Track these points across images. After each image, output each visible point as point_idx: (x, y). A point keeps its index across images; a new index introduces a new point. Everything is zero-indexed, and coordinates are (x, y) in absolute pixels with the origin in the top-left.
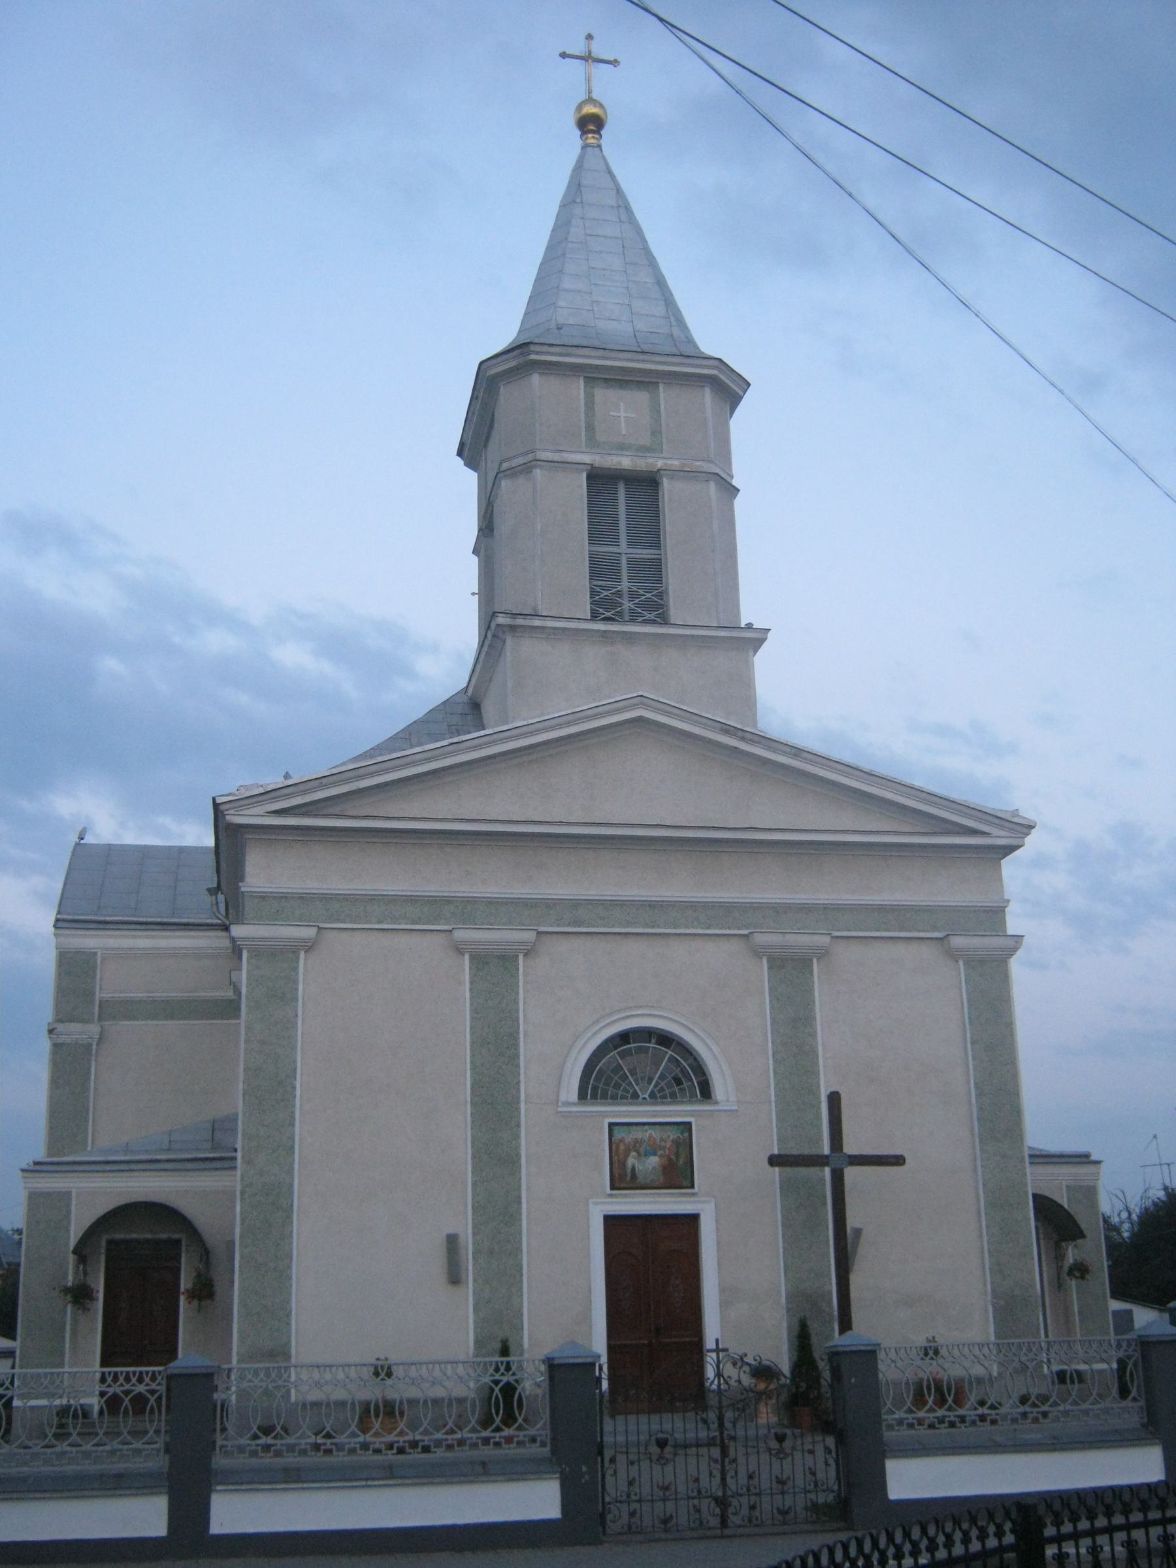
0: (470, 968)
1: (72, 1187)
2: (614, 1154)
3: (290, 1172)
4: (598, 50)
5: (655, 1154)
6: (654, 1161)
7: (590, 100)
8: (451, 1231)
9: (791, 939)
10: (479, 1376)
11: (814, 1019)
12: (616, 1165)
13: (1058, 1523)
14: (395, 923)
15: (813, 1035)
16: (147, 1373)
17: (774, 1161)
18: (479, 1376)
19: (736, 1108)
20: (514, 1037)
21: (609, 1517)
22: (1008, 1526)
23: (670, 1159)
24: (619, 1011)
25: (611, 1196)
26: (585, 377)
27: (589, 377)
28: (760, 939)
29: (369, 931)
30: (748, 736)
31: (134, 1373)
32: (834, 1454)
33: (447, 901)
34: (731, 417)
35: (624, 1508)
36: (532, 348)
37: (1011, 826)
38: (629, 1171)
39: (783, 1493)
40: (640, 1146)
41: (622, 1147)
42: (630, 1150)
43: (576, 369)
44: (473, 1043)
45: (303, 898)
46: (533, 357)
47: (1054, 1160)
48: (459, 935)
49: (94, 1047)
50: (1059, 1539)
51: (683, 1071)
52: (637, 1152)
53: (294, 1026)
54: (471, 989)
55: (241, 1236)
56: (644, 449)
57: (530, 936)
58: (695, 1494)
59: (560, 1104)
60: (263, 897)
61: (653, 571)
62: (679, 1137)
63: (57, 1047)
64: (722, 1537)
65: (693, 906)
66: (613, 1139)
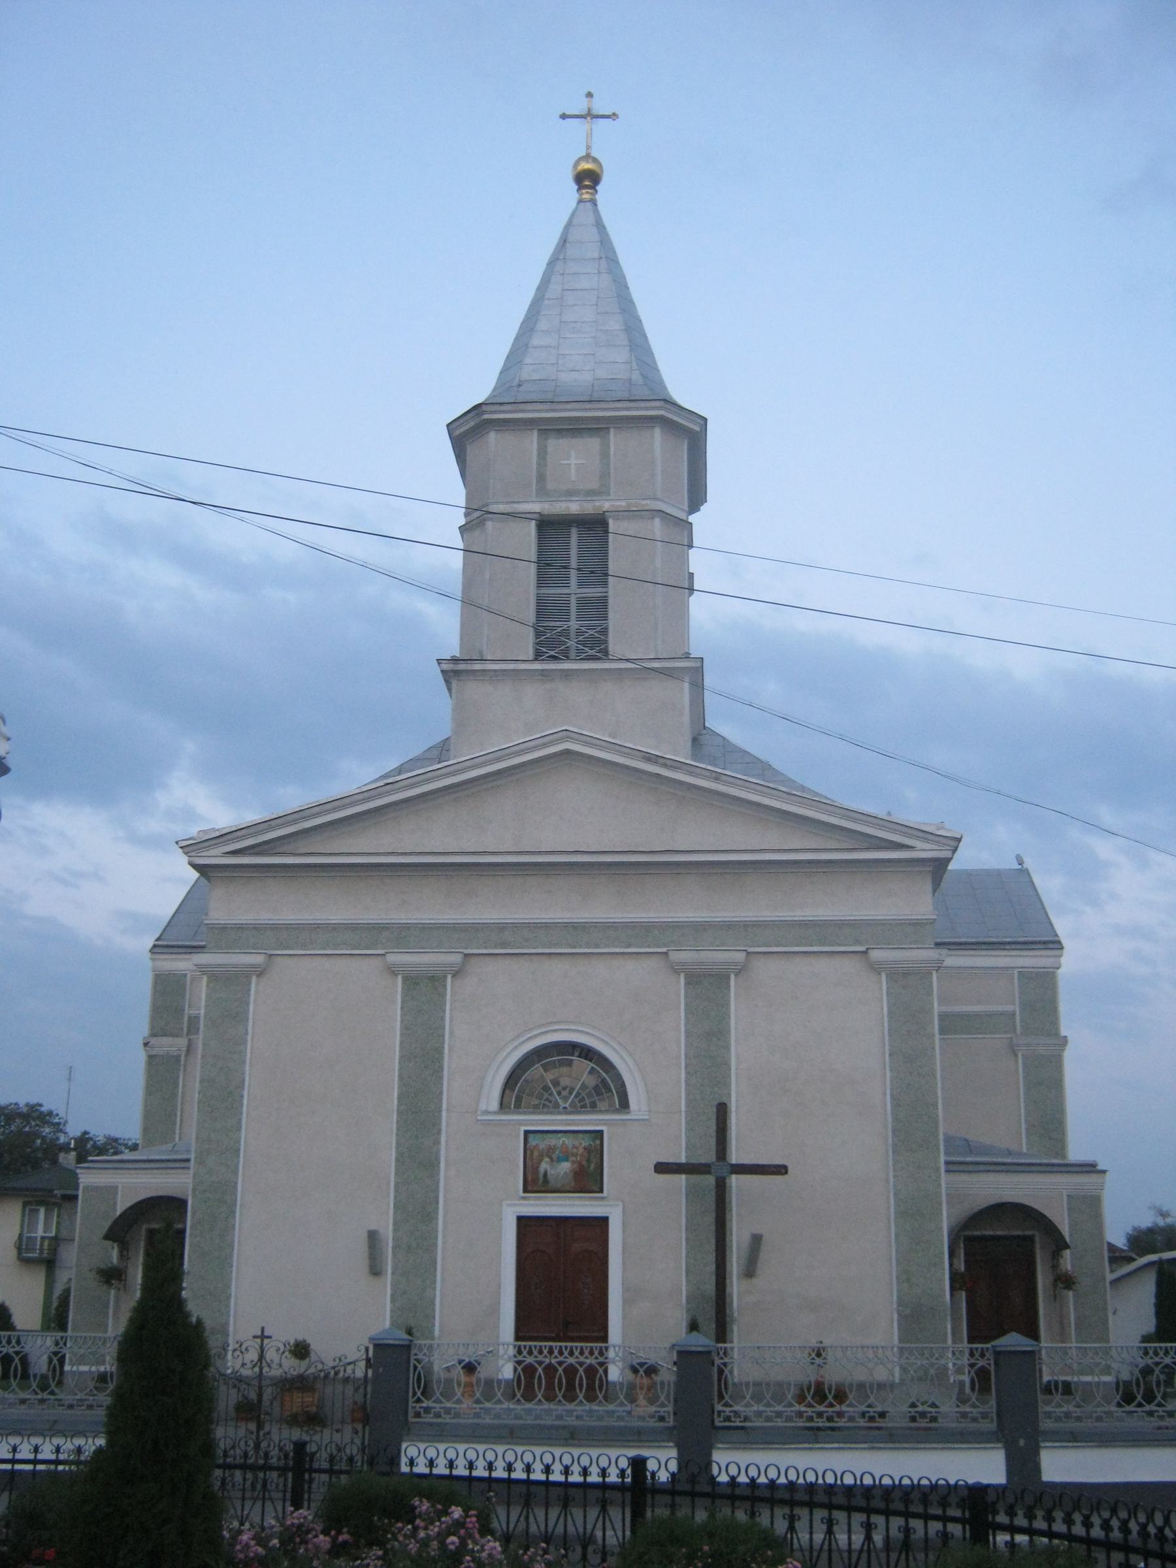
2: (528, 1160)
3: (236, 1172)
4: (599, 107)
5: (567, 1160)
6: (566, 1166)
7: (588, 157)
8: (372, 1228)
9: (705, 956)
10: (813, 1359)
11: (729, 1031)
12: (529, 1163)
15: (728, 1048)
16: (577, 1347)
18: (813, 1359)
19: (647, 1117)
20: (439, 1051)
24: (540, 1026)
25: (524, 1198)
26: (539, 430)
27: (542, 430)
28: (675, 956)
29: (363, 957)
30: (669, 763)
31: (525, 1347)
32: (360, 1435)
36: (484, 408)
37: (937, 838)
41: (536, 1154)
42: (543, 1156)
43: (529, 423)
44: (401, 1057)
45: (257, 928)
46: (486, 416)
47: (1033, 1168)
48: (391, 958)
49: (183, 1058)
51: (604, 1081)
53: (245, 1042)
54: (402, 1008)
55: (191, 1227)
56: (591, 493)
57: (457, 959)
59: (479, 1113)
61: (598, 608)
62: (591, 1145)
63: (151, 1058)
65: (613, 926)
66: (528, 1145)
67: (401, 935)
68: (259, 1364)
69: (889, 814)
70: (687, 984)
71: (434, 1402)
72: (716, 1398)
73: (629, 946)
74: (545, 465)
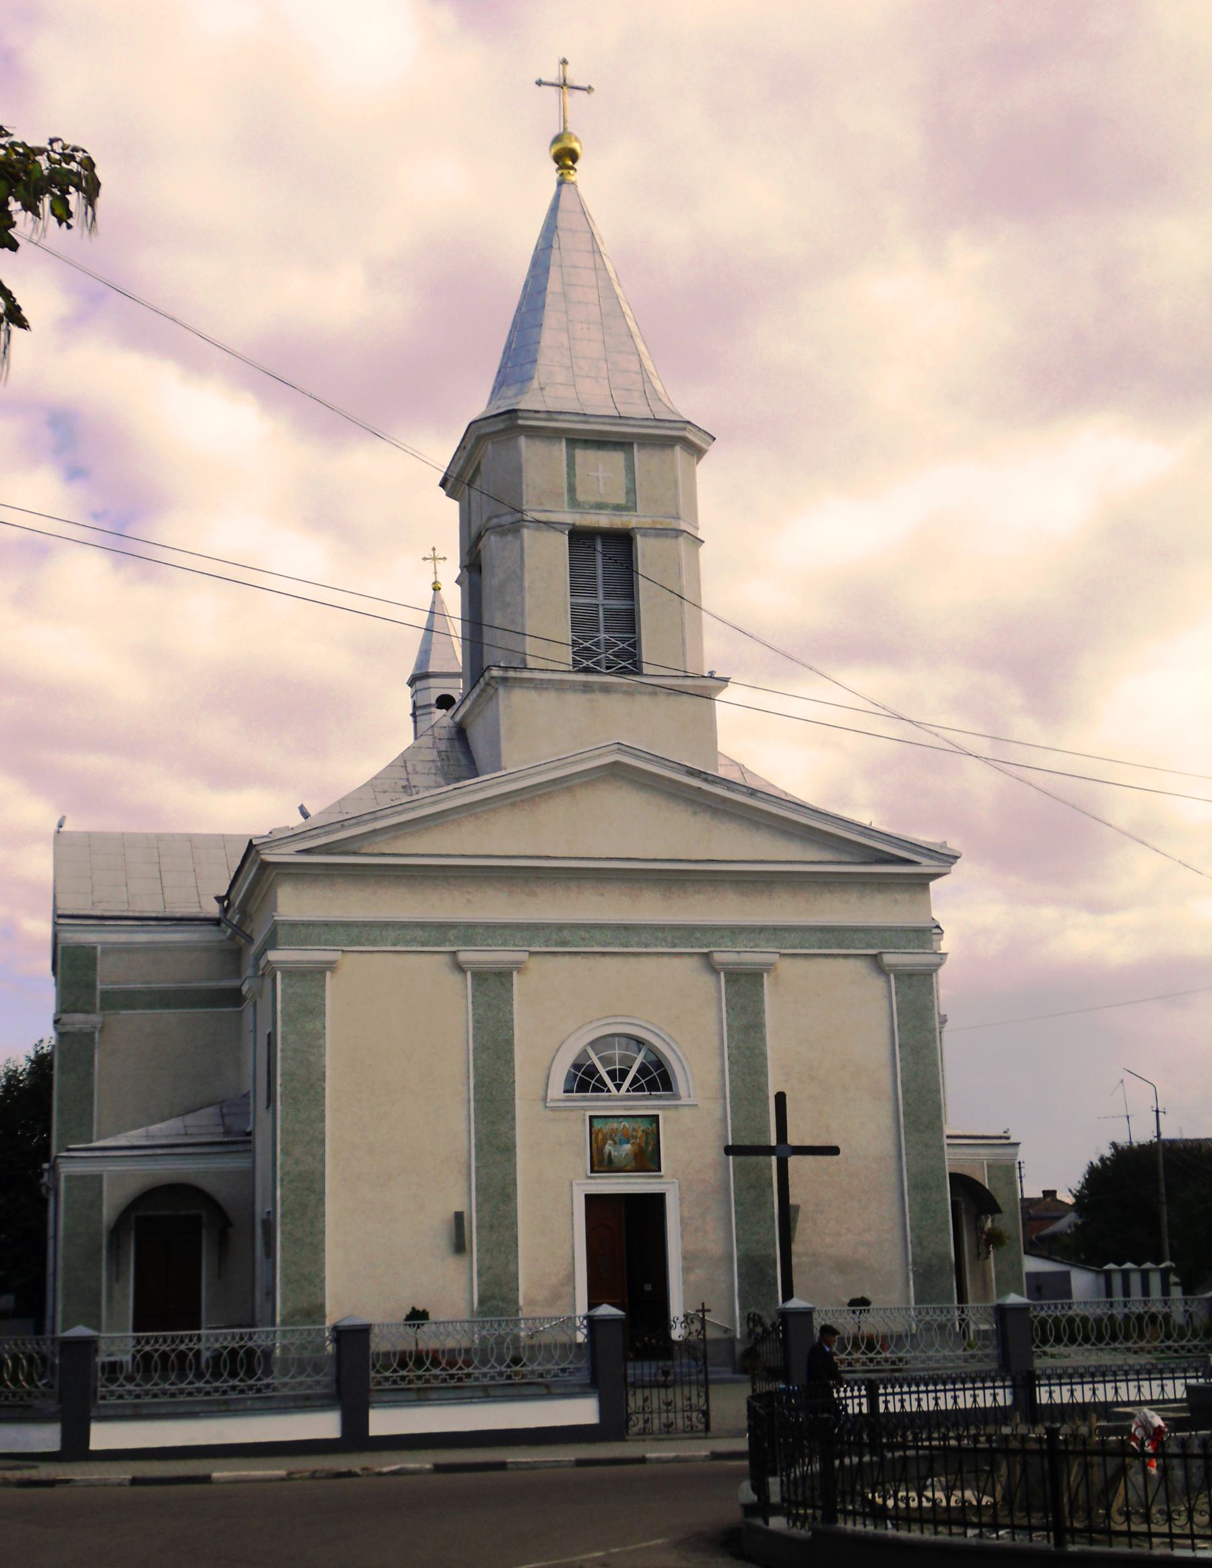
0: (472, 984)
1: (103, 1171)
4: (574, 78)
5: (628, 1142)
6: (627, 1147)
12: (594, 1146)
13: (885, 1388)
14: (407, 946)
15: (763, 1039)
17: (729, 1150)
21: (631, 1423)
22: (863, 1388)
23: (640, 1146)
25: (590, 1178)
30: (710, 778)
33: (452, 926)
34: (697, 463)
35: (640, 1416)
38: (606, 1156)
39: (668, 1411)
40: (616, 1135)
41: (600, 1136)
46: (520, 422)
50: (886, 1394)
52: (613, 1140)
53: (323, 1036)
56: (618, 508)
58: (688, 1408)
60: (294, 925)
61: (629, 621)
64: (706, 1438)
66: (593, 1129)
67: (469, 932)
68: (702, 1332)
69: (871, 824)
70: (727, 982)
71: (474, 1368)
72: (371, 1367)
73: (674, 946)
74: (575, 476)
